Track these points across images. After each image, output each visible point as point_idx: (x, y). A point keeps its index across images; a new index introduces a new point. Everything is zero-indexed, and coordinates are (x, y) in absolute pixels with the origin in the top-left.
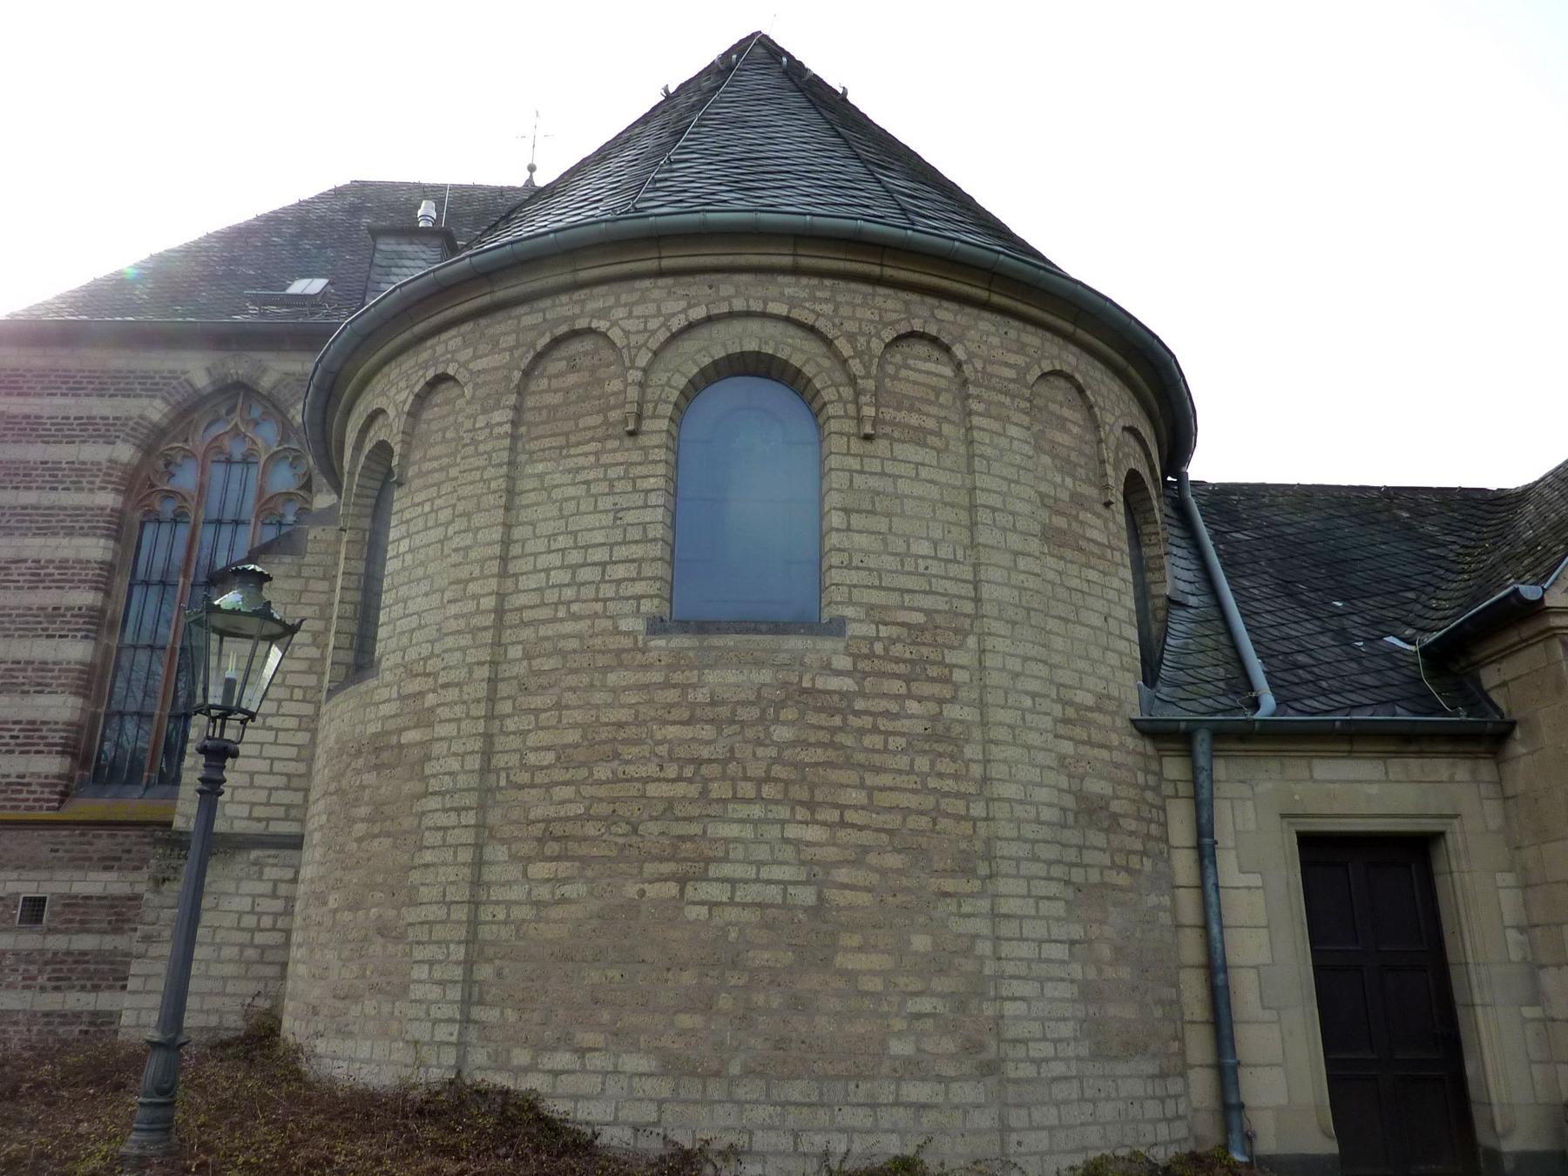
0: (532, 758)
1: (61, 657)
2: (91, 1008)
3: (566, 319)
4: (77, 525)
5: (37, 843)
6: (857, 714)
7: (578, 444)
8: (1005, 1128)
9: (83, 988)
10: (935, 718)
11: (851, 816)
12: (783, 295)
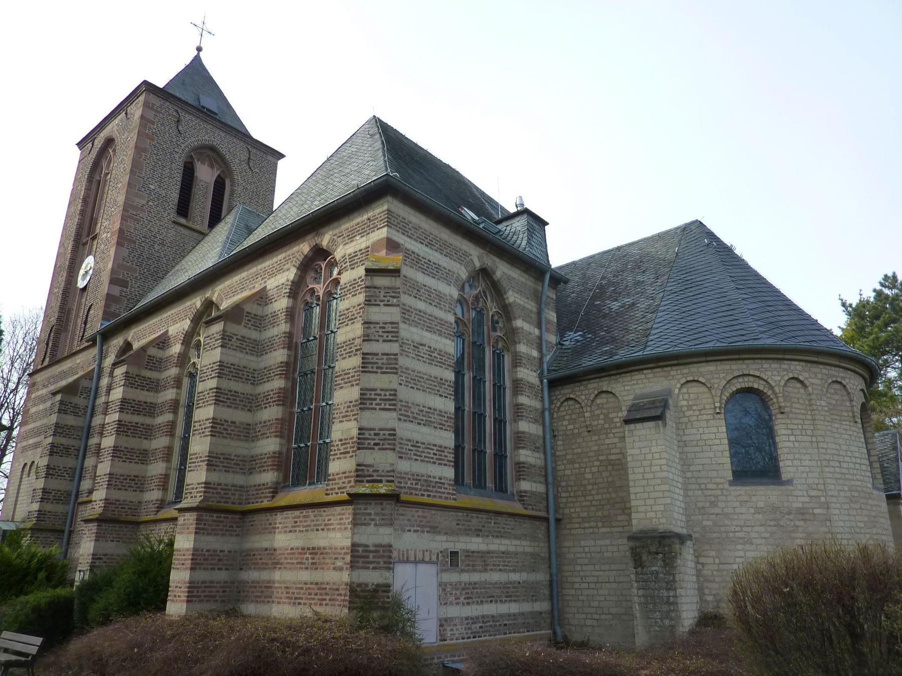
6: (866, 515)
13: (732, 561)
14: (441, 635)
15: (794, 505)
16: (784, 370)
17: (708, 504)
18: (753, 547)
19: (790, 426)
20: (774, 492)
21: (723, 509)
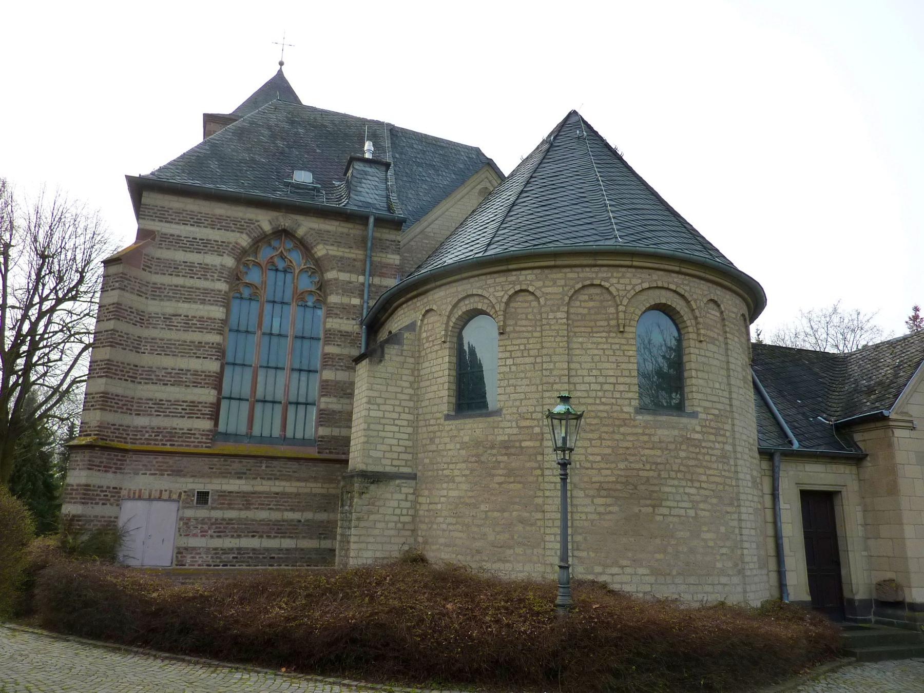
0: (591, 458)
1: (204, 369)
2: (237, 546)
3: (589, 279)
4: (207, 299)
5: (201, 464)
6: (703, 448)
7: (597, 332)
8: (745, 592)
9: (232, 536)
10: (723, 449)
11: (703, 485)
12: (675, 281)
13: (437, 500)
14: (177, 560)
15: (500, 438)
19: (509, 348)
20: (481, 425)
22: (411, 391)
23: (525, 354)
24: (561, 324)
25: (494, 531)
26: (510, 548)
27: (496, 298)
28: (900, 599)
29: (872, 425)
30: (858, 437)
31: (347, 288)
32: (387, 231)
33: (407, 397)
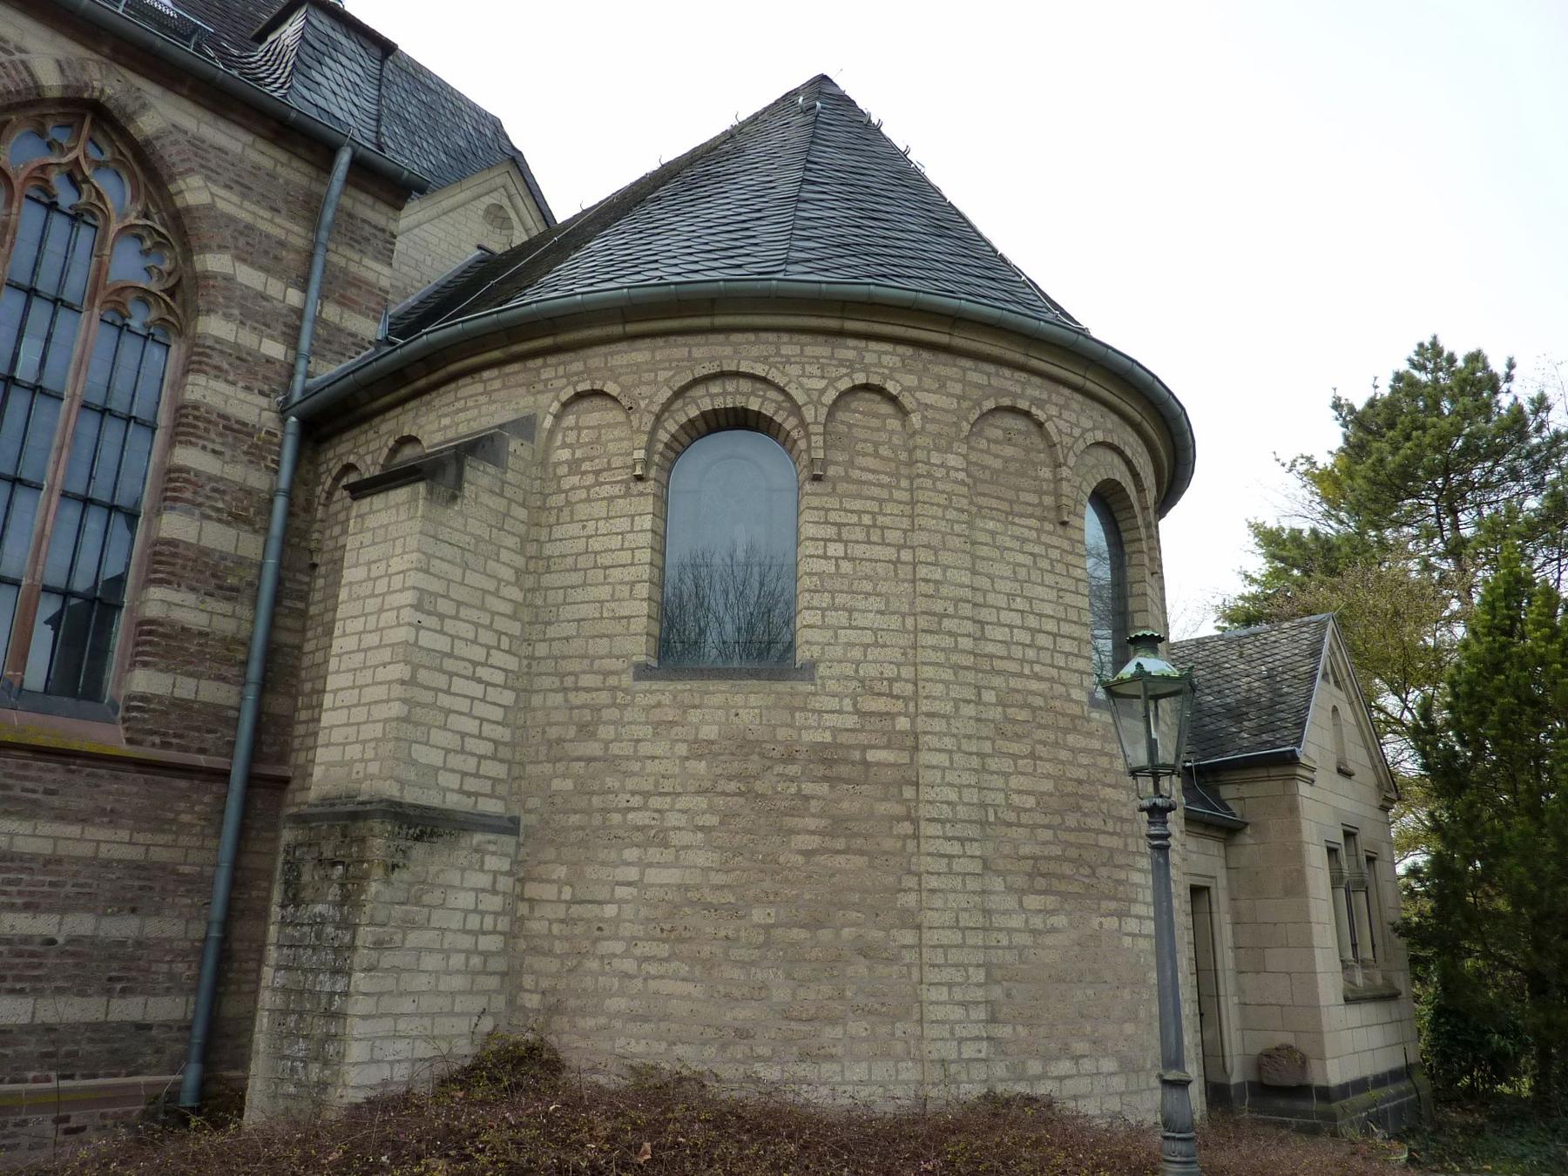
0: (1015, 799)
7: (1021, 516)
13: (603, 893)
15: (807, 736)
16: (842, 363)
17: (572, 732)
18: (668, 855)
19: (833, 517)
20: (753, 700)
21: (607, 743)
22: (517, 595)
23: (874, 538)
24: (956, 481)
25: (789, 976)
26: (833, 1021)
27: (808, 391)
28: (1304, 1083)
29: (1262, 773)
30: (1227, 792)
31: (253, 311)
32: (370, 200)
33: (507, 608)
